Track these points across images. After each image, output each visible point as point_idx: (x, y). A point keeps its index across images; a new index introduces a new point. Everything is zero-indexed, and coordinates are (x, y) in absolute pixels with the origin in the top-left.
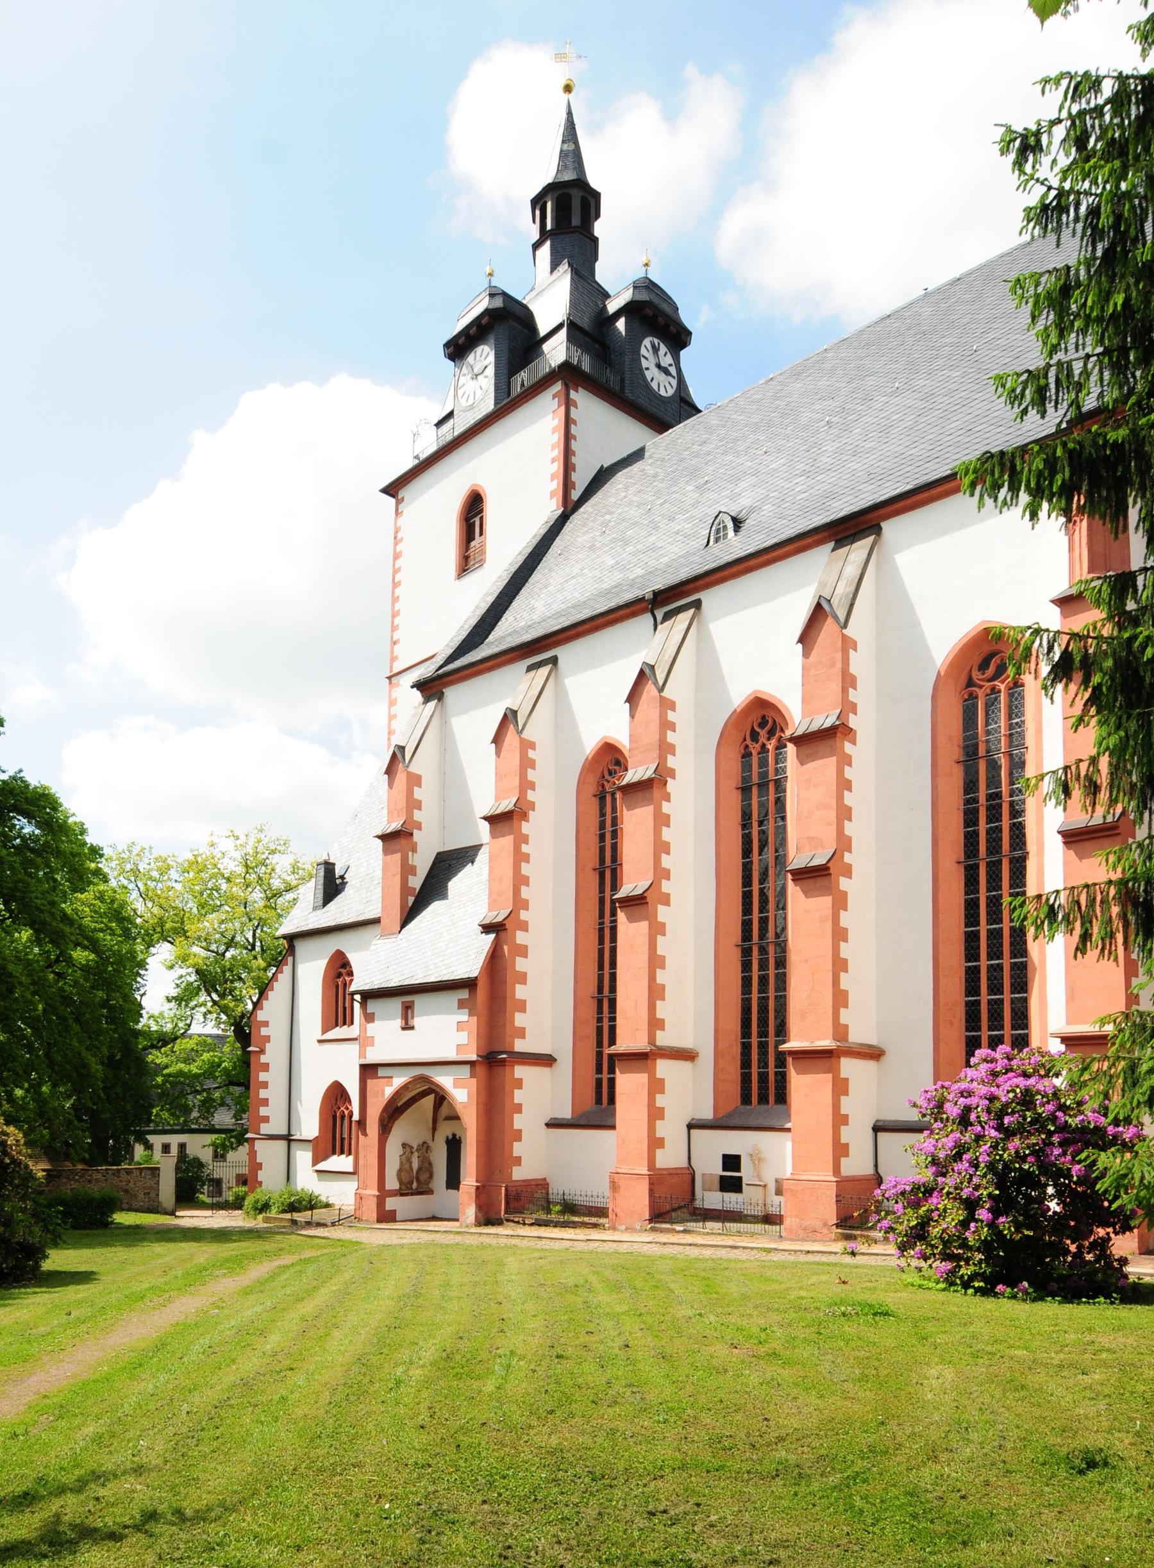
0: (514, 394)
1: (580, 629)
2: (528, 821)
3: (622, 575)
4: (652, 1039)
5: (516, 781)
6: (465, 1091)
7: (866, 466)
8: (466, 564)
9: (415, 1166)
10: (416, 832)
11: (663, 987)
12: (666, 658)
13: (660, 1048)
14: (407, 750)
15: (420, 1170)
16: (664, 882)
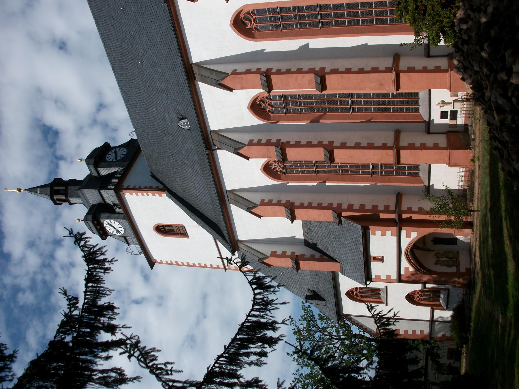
0: (123, 212)
1: (217, 181)
2: (294, 203)
3: (197, 165)
4: (391, 148)
5: (277, 208)
6: (412, 233)
7: (168, 71)
9: (445, 259)
10: (296, 254)
12: (232, 144)
15: (447, 257)
16: (324, 143)
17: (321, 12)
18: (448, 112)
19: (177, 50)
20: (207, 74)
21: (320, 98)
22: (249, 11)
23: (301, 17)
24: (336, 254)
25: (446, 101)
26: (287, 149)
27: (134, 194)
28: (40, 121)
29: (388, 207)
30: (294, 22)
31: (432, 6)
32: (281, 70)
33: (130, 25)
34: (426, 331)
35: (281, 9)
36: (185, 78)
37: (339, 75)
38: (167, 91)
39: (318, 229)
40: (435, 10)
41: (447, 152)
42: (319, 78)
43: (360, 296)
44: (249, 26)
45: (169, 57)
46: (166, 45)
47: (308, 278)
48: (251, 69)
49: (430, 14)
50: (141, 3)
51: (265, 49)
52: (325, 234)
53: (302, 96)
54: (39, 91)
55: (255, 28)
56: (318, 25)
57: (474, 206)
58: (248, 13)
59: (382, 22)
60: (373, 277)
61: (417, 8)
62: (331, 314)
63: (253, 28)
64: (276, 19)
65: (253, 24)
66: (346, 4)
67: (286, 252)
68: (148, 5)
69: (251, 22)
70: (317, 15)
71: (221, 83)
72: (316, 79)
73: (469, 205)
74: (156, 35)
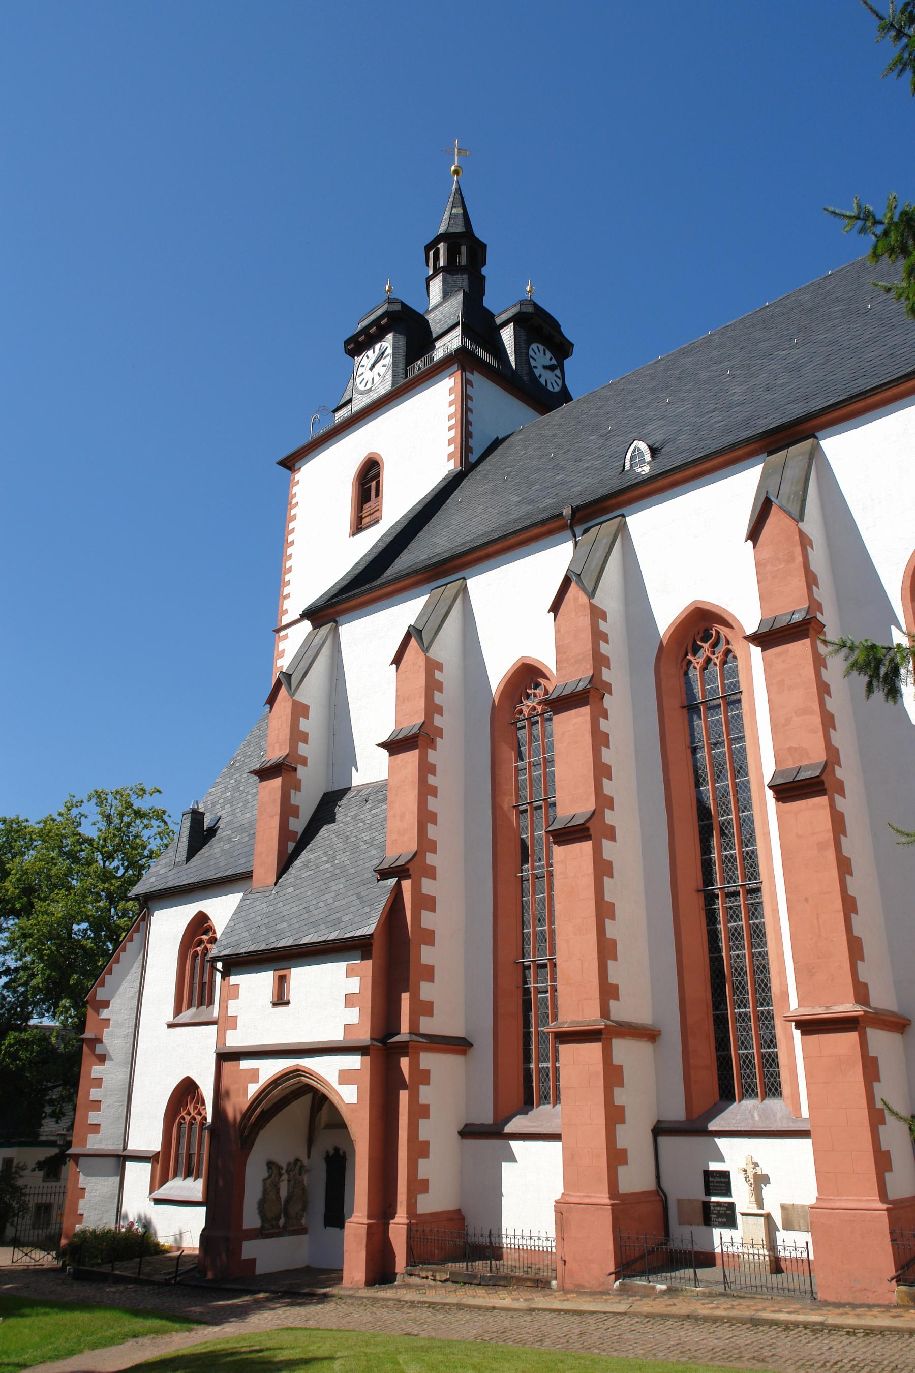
4: (605, 1012)
5: (421, 704)
8: (358, 526)
9: (284, 1193)
10: (300, 768)
11: (614, 942)
13: (620, 1024)
14: (293, 678)
18: (731, 1196)
21: (737, 801)
24: (298, 873)
25: (766, 1191)
26: (585, 710)
27: (453, 397)
29: (430, 1013)
34: (94, 1143)
37: (831, 835)
39: (367, 822)
41: (604, 1198)
42: (818, 774)
43: (196, 952)
47: (248, 815)
52: (354, 839)
53: (741, 747)
57: (434, 1287)
60: (234, 980)
62: (153, 880)
67: (306, 741)
72: (808, 767)
73: (440, 1271)
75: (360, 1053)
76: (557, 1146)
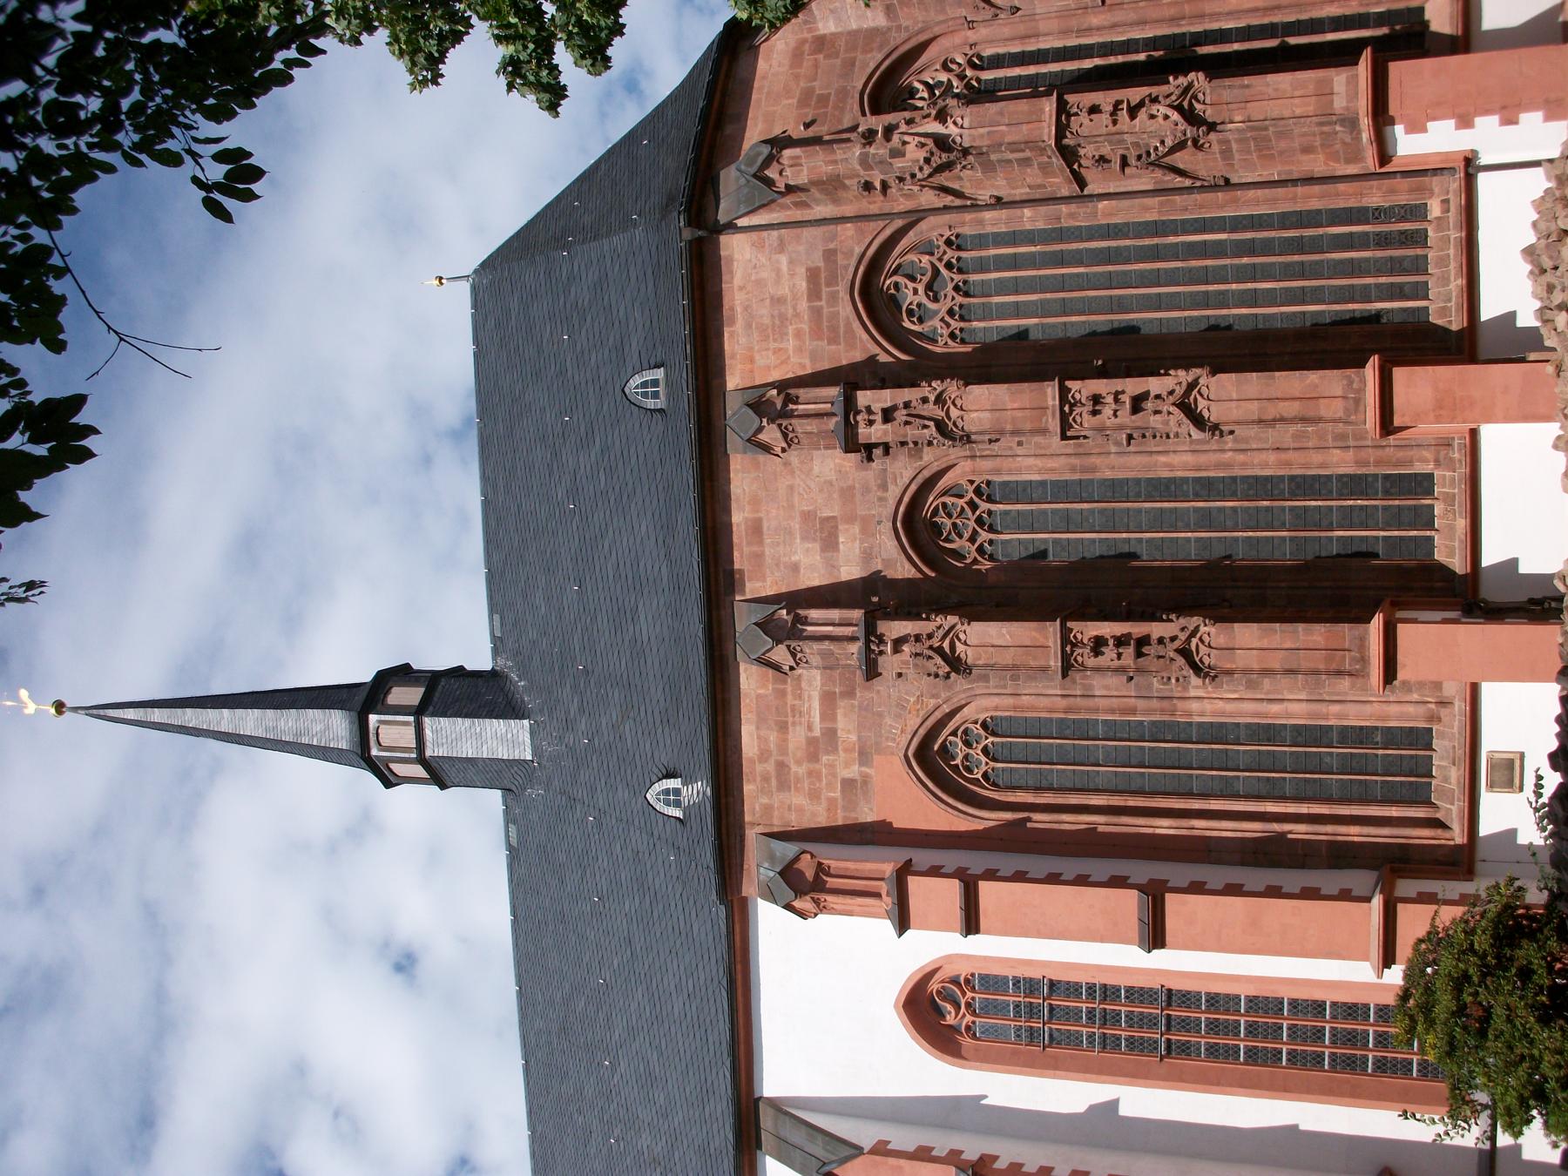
17: (1170, 1013)
19: (725, 1048)
20: (797, 1136)
22: (959, 976)
23: (1110, 1019)
28: (273, 1156)
30: (1085, 1030)
31: (1509, 1008)
32: (1021, 1165)
33: (609, 949)
35: (1053, 984)
36: (731, 1136)
38: (668, 1167)
40: (1518, 1023)
44: (950, 1019)
45: (696, 1066)
46: (696, 1026)
48: (934, 1148)
49: (1502, 1033)
50: (652, 894)
51: (985, 1097)
54: (300, 1069)
55: (968, 1028)
56: (1156, 1048)
58: (955, 981)
59: (1352, 1065)
61: (1461, 1010)
63: (960, 1025)
64: (1032, 1011)
65: (964, 1015)
66: (1246, 997)
68: (673, 904)
69: (957, 1007)
70: (1155, 1018)
71: (835, 1171)
74: (674, 995)
75: (1388, 128)
76: (1489, 691)
